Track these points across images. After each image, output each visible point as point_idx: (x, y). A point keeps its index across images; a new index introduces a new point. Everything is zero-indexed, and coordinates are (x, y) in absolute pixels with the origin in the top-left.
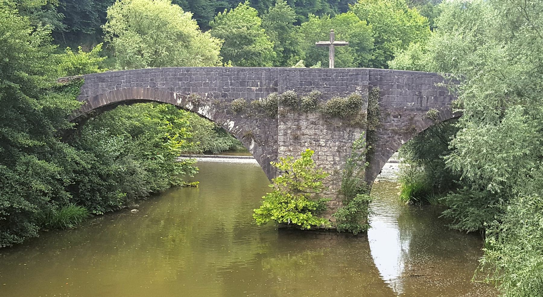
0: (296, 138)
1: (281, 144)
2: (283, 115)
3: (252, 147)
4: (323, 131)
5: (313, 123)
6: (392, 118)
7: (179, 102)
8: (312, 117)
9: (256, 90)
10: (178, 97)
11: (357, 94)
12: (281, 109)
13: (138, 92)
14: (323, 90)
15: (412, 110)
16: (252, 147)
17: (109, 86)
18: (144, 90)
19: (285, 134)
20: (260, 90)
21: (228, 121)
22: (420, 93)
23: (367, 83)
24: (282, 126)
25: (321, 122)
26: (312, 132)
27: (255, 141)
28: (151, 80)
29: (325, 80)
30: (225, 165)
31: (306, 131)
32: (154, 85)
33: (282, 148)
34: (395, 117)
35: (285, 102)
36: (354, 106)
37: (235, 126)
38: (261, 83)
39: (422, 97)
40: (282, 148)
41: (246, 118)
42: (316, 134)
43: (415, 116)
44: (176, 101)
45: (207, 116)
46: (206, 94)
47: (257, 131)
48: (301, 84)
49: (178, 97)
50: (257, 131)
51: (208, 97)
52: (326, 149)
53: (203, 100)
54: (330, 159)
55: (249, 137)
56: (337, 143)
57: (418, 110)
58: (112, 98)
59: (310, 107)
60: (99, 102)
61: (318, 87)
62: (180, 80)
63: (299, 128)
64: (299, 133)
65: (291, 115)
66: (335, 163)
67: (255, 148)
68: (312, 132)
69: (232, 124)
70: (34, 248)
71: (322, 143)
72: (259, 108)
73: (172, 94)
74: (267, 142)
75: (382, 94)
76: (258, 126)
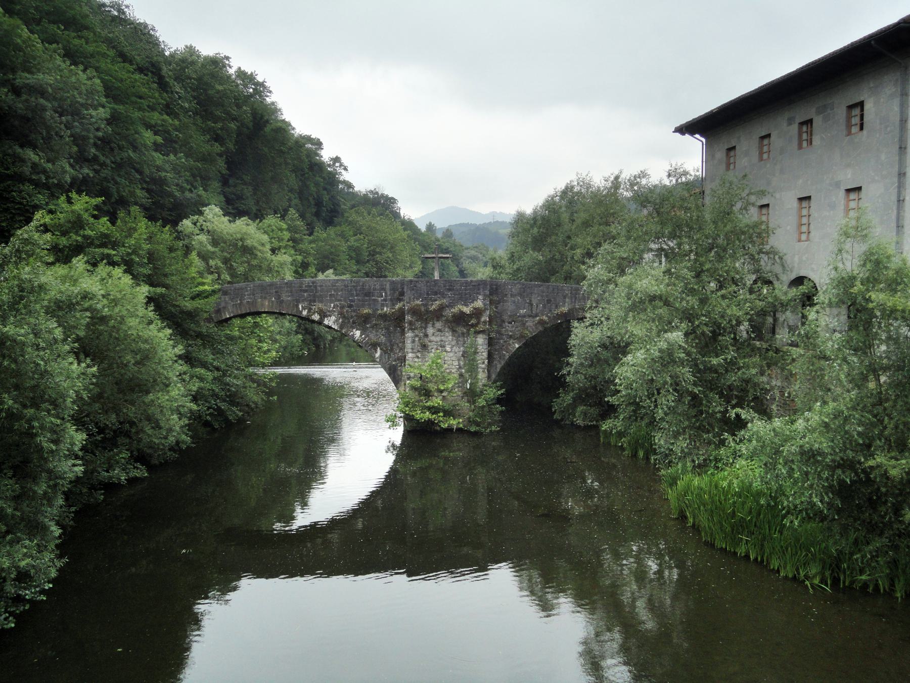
0: (424, 347)
1: (410, 350)
2: (411, 323)
3: (378, 355)
4: (448, 337)
5: (439, 330)
6: (507, 324)
7: (305, 313)
8: (439, 325)
9: (382, 300)
10: (304, 308)
11: (479, 304)
12: (408, 318)
13: (262, 305)
14: (448, 299)
15: (524, 316)
16: (378, 355)
17: (232, 300)
18: (269, 302)
19: (413, 342)
20: (385, 300)
21: (354, 330)
22: (531, 301)
23: (487, 292)
24: (409, 334)
25: (447, 329)
26: (438, 339)
27: (381, 349)
28: (276, 292)
29: (449, 290)
30: (290, 376)
31: (433, 338)
32: (278, 297)
33: (410, 355)
34: (510, 323)
35: (414, 312)
36: (477, 313)
37: (361, 336)
38: (386, 293)
39: (532, 305)
40: (410, 355)
41: (372, 327)
42: (442, 341)
43: (527, 321)
44: (301, 312)
45: (333, 327)
46: (332, 305)
47: (383, 339)
48: (428, 294)
49: (304, 308)
50: (383, 339)
51: (334, 308)
52: (451, 354)
53: (329, 311)
54: (456, 363)
55: (375, 345)
56: (462, 348)
57: (530, 316)
58: (235, 312)
59: (438, 315)
60: (221, 314)
61: (443, 296)
62: (305, 291)
63: (426, 336)
64: (426, 340)
65: (418, 324)
66: (460, 368)
67: (381, 355)
68: (438, 339)
69: (357, 334)
70: (801, 415)
71: (448, 349)
72: (384, 317)
73: (297, 306)
74: (392, 350)
75: (499, 302)
76: (383, 335)
